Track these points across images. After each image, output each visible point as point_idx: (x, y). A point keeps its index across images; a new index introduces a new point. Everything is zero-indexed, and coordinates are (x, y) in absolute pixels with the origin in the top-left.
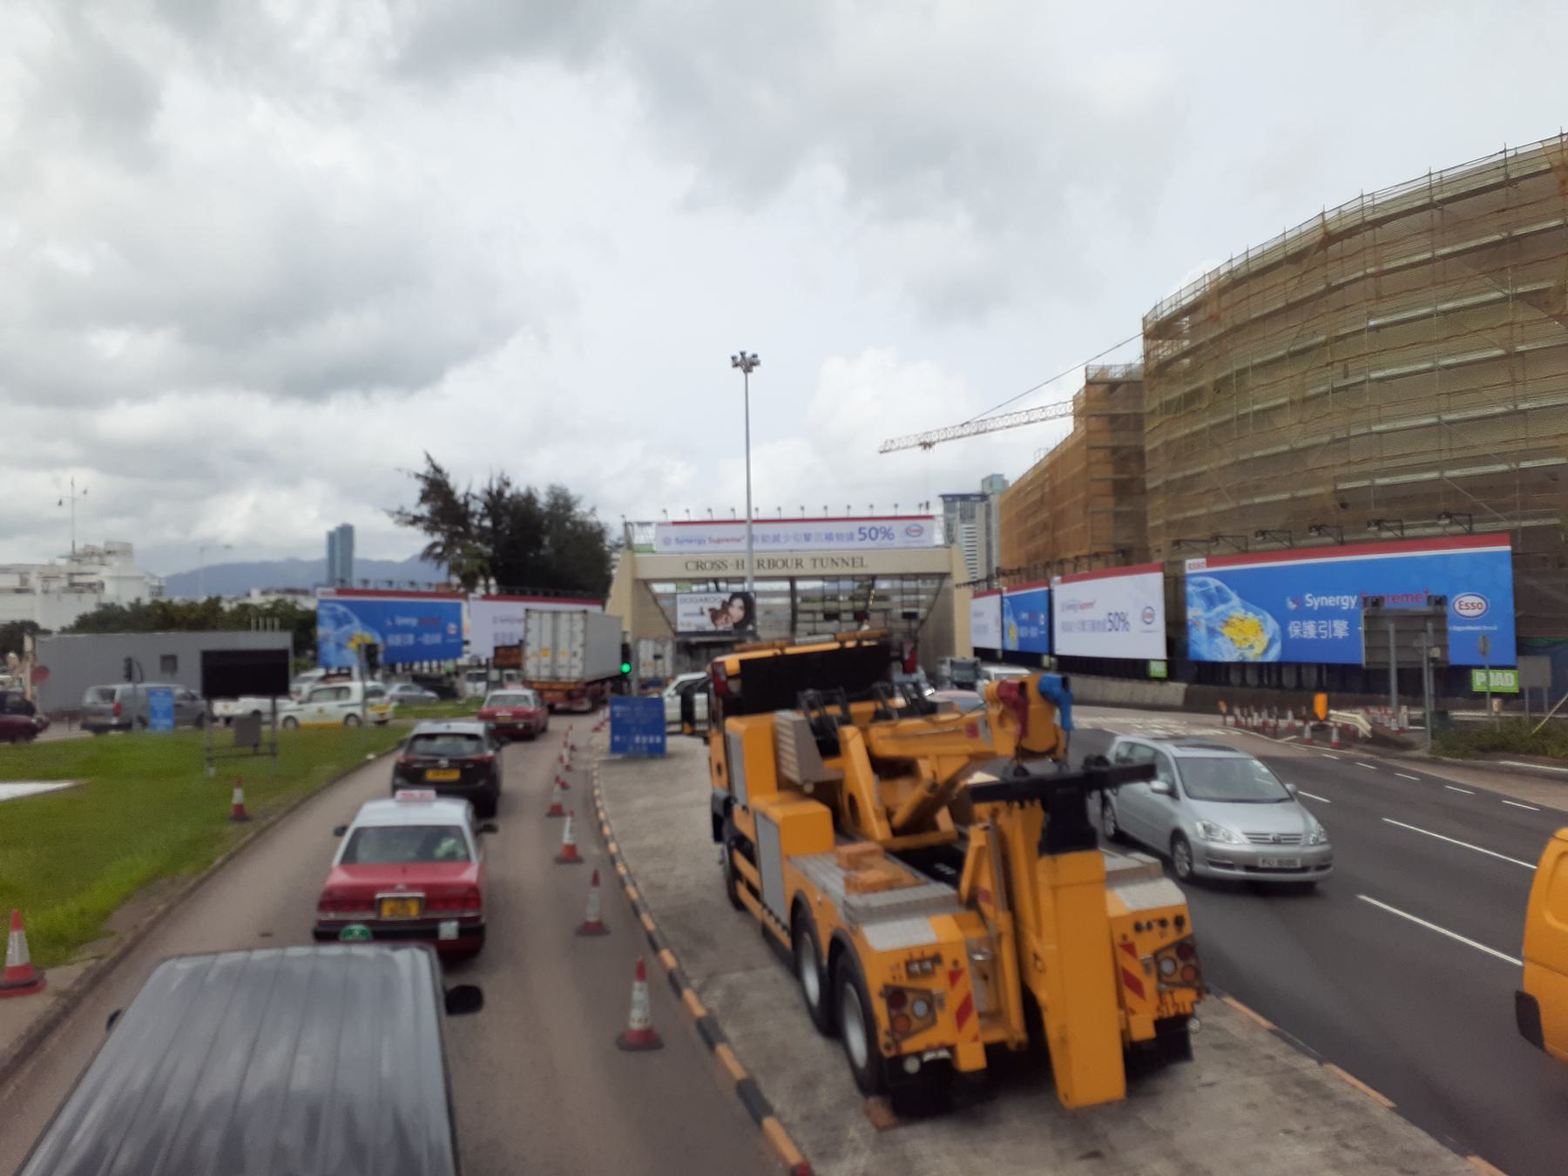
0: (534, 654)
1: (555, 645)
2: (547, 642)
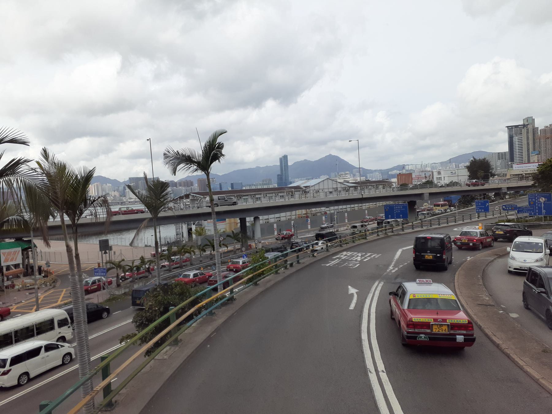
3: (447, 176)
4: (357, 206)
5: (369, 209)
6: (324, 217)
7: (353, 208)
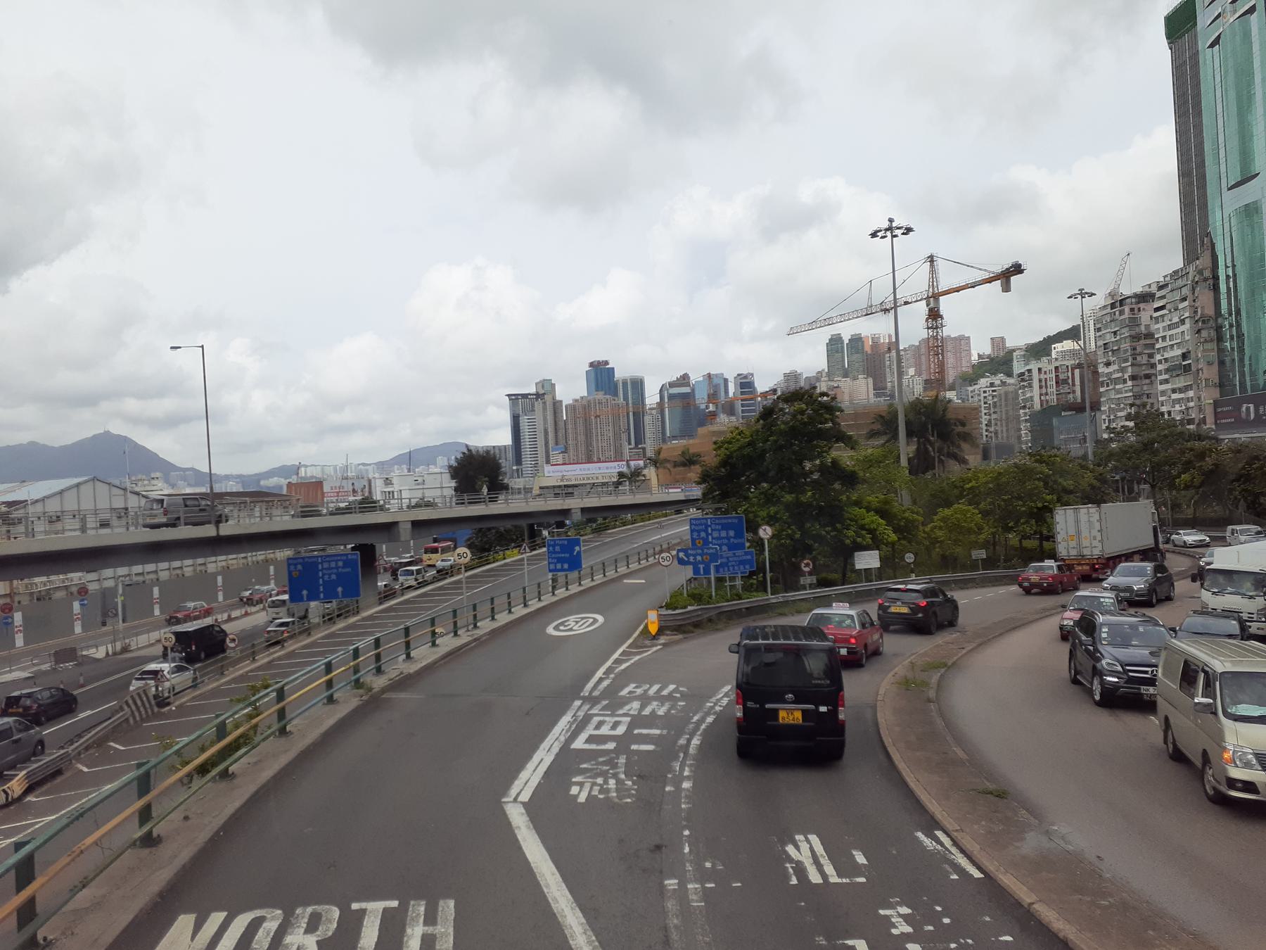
0: (1064, 540)
1: (1079, 533)
2: (1072, 531)
3: (407, 488)
4: (191, 564)
5: (226, 571)
6: (76, 606)
7: (179, 572)
